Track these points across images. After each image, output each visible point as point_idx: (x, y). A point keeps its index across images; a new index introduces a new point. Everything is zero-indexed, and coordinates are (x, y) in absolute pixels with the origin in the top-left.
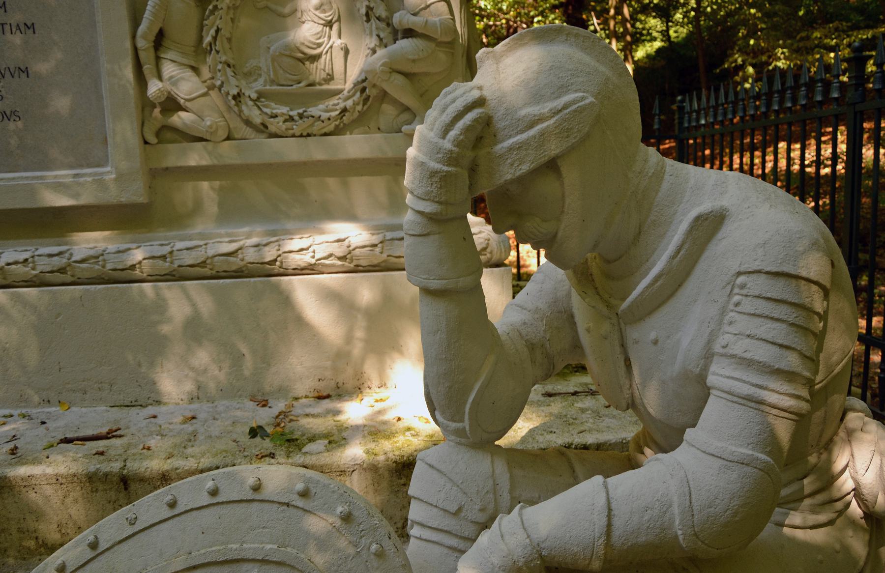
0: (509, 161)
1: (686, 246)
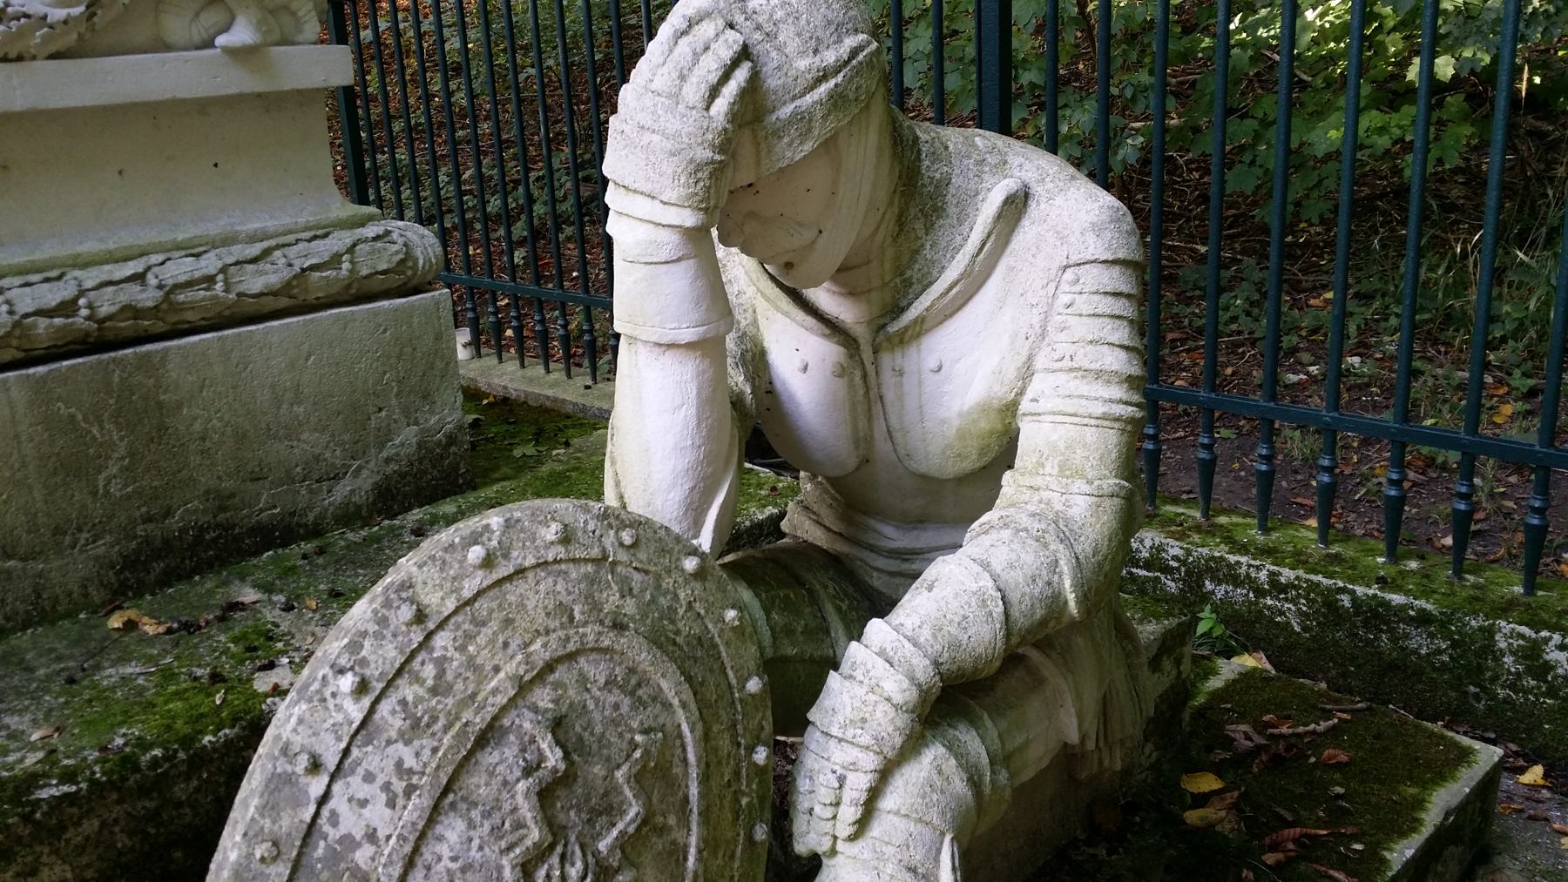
0: (786, 140)
1: (993, 238)
